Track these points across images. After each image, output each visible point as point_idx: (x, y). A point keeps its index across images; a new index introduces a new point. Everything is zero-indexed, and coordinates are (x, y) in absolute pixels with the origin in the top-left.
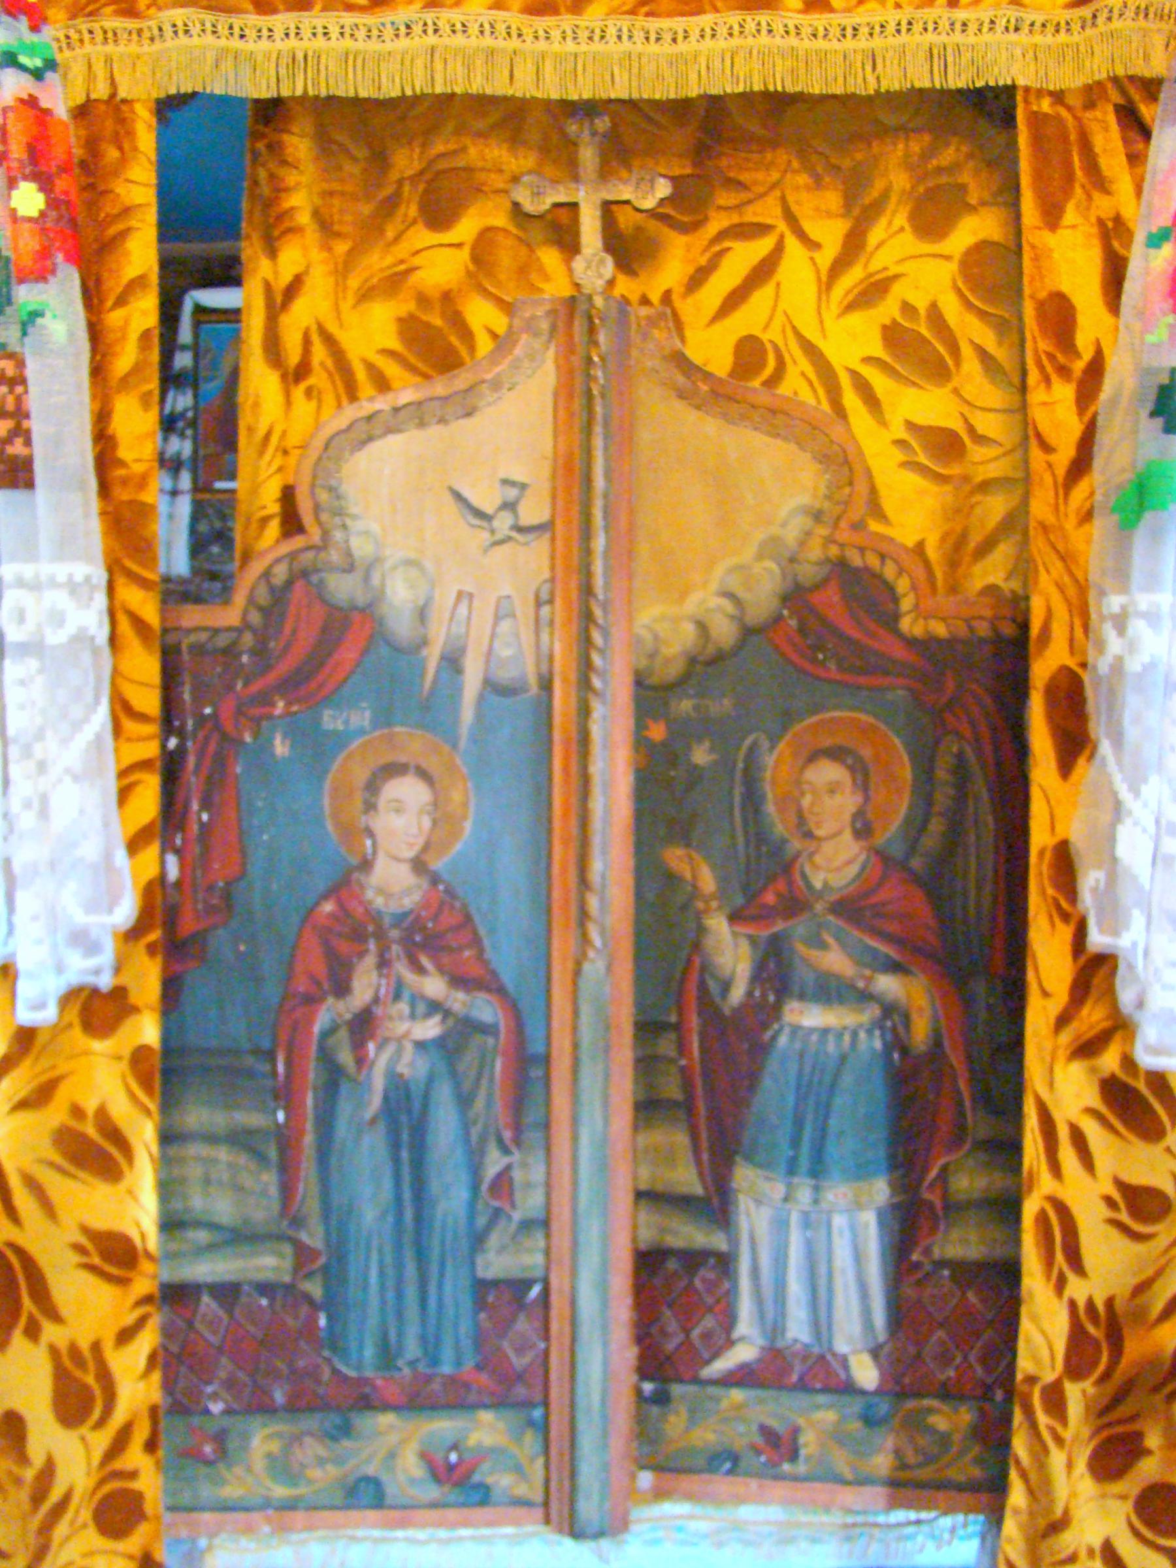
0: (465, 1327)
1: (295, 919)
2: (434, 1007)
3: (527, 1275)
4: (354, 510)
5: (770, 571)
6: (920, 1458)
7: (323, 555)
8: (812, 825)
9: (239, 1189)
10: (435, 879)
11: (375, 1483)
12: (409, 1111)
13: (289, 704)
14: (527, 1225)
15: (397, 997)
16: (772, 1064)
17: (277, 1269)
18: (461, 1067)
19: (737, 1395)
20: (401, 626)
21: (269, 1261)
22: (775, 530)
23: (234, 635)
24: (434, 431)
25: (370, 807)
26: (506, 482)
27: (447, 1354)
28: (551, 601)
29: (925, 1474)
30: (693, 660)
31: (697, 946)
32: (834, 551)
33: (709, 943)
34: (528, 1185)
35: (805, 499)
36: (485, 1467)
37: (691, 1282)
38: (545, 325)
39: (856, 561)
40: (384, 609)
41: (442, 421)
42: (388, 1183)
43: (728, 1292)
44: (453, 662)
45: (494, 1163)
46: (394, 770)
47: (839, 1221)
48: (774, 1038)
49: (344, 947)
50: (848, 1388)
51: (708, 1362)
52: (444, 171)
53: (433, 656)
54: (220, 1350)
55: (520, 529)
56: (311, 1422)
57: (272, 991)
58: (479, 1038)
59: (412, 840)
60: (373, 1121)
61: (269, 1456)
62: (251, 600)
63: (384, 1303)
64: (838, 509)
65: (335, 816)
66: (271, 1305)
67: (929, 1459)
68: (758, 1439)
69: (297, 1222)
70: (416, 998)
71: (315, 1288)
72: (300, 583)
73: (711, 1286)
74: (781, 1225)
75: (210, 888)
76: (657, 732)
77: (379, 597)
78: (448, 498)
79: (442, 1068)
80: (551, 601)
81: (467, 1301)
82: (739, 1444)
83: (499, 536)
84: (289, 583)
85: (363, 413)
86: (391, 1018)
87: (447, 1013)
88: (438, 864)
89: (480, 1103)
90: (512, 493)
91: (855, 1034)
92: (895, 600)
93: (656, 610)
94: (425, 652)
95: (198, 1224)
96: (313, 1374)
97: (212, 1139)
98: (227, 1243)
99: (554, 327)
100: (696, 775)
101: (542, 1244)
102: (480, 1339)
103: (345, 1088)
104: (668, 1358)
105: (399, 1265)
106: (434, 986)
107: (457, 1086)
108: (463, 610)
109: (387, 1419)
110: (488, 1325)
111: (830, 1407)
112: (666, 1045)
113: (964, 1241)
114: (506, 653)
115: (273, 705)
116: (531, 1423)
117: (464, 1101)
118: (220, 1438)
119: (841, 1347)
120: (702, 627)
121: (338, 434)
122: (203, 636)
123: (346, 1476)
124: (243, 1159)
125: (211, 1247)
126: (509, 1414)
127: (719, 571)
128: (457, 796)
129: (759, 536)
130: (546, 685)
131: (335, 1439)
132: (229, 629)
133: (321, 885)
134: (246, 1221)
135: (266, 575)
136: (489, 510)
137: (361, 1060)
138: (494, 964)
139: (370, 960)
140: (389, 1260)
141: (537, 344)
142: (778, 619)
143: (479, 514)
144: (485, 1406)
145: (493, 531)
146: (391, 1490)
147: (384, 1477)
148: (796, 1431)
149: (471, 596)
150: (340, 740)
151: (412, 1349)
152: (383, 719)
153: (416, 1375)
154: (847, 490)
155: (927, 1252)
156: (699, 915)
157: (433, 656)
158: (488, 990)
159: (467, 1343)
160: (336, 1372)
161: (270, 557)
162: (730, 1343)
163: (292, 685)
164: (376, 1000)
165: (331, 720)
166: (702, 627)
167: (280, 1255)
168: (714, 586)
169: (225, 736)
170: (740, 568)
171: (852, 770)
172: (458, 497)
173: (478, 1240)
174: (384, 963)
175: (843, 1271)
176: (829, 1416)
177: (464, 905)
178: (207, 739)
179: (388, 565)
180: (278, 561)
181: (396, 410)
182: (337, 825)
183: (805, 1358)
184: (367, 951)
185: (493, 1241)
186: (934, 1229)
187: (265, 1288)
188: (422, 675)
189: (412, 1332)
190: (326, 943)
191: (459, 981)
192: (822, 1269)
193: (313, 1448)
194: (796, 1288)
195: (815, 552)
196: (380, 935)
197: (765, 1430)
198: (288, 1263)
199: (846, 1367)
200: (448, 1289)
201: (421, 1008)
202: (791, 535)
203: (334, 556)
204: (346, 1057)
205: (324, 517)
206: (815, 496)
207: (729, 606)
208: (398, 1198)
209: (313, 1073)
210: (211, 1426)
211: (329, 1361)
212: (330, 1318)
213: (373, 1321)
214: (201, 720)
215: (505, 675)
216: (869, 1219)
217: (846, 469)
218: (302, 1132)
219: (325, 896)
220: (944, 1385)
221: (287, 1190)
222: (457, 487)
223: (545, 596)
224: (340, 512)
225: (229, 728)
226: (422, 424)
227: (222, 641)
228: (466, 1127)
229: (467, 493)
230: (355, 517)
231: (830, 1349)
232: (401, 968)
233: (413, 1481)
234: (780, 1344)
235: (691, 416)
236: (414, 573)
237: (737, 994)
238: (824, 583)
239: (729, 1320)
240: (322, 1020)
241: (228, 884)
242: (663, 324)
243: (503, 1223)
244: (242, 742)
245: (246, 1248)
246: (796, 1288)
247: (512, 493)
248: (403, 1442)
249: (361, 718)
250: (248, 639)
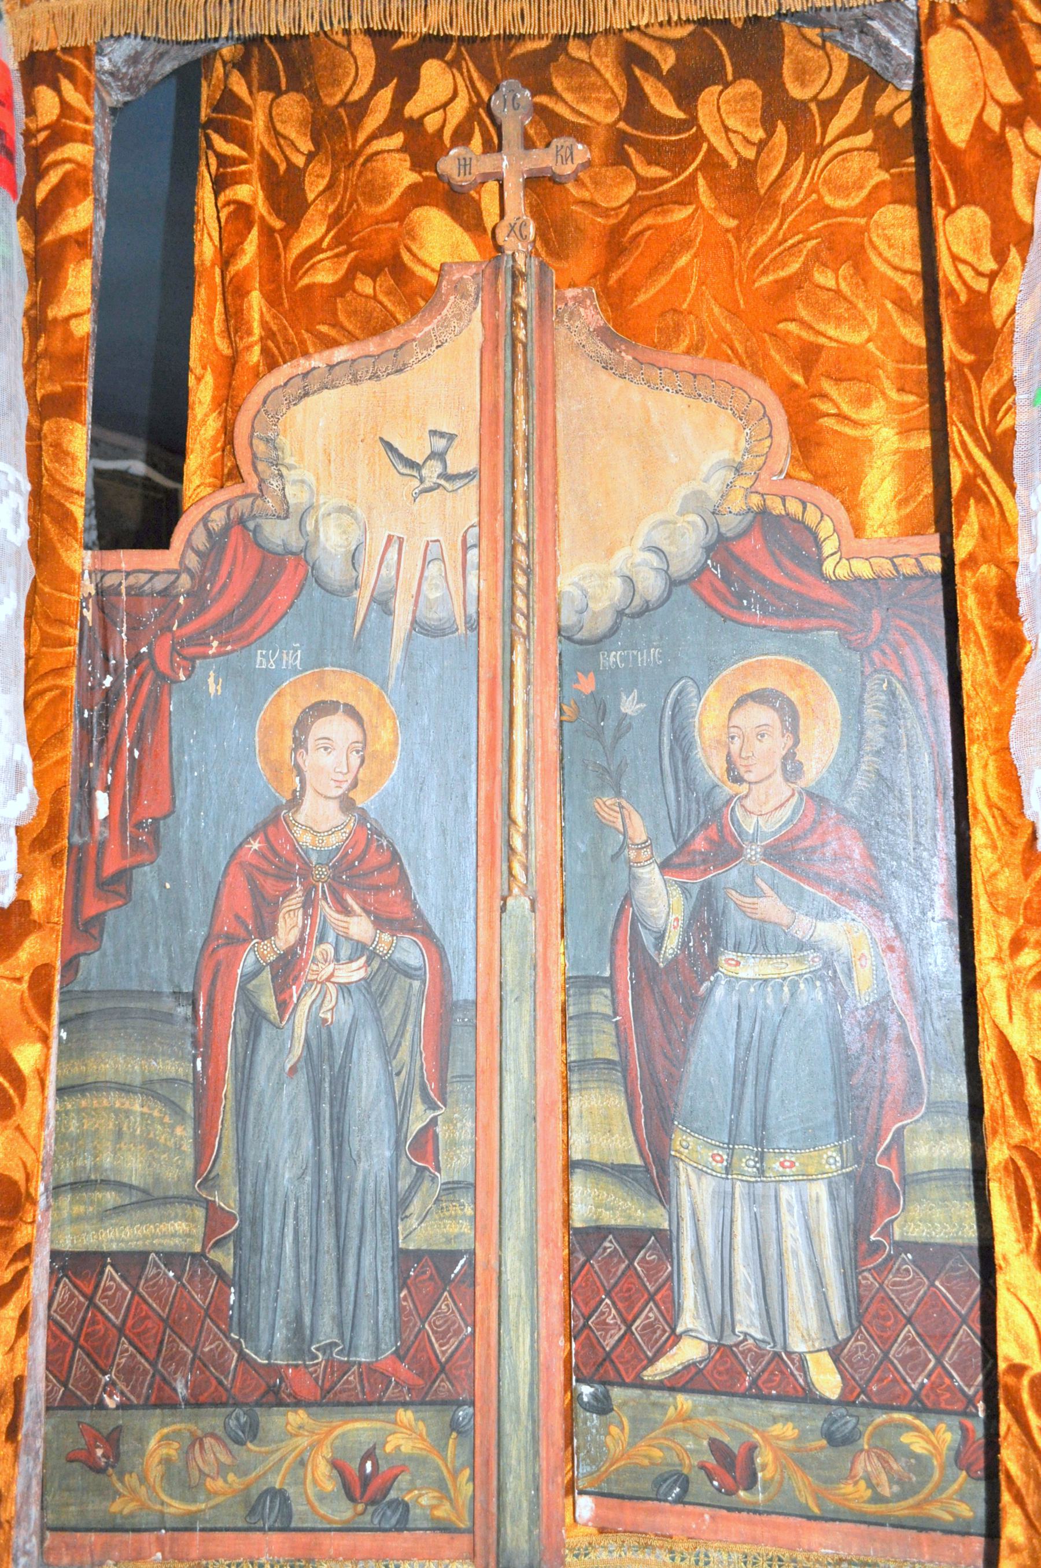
0: (386, 1305)
1: (223, 859)
2: (360, 949)
3: (454, 1246)
4: (289, 460)
5: (693, 524)
6: (896, 1488)
7: (259, 502)
8: (742, 770)
9: (151, 1144)
10: (363, 816)
11: (280, 1496)
12: (331, 1059)
13: (223, 644)
14: (452, 1188)
15: (321, 940)
16: (710, 1019)
17: (188, 1235)
18: (386, 1013)
19: (684, 1401)
20: (334, 571)
21: (180, 1226)
22: (696, 485)
23: (173, 577)
24: (367, 386)
25: (299, 744)
26: (433, 433)
27: (365, 1338)
28: (478, 545)
29: (900, 1509)
30: (620, 613)
31: (628, 898)
32: (755, 500)
33: (640, 893)
34: (453, 1143)
35: (726, 454)
36: (404, 1479)
37: (631, 1265)
38: (472, 288)
39: (776, 507)
40: (316, 554)
41: (375, 376)
42: (307, 1141)
43: (670, 1276)
44: (383, 603)
45: (418, 1118)
46: (323, 709)
47: (787, 1193)
48: (710, 991)
49: (270, 886)
50: (808, 1396)
51: (652, 1361)
52: (377, 153)
53: (364, 597)
54: (121, 1330)
55: (450, 478)
56: (213, 1420)
57: (197, 933)
58: (402, 981)
59: (340, 777)
60: (293, 1070)
61: (167, 1461)
62: (188, 543)
63: (298, 1276)
64: (760, 461)
65: (265, 751)
66: (178, 1278)
67: (907, 1491)
68: (711, 1460)
69: (209, 1181)
70: (344, 937)
71: (226, 1259)
72: (236, 530)
73: (652, 1270)
74: (725, 1200)
75: (139, 825)
76: (587, 685)
77: (310, 543)
78: (380, 448)
79: (366, 1014)
80: (478, 545)
81: (387, 1277)
82: (689, 1465)
83: (427, 484)
84: (226, 530)
85: (300, 370)
86: (315, 961)
87: (373, 955)
88: (362, 801)
89: (404, 1054)
90: (441, 444)
91: (794, 985)
92: (818, 545)
93: (584, 568)
94: (356, 594)
95: (106, 1183)
96: (219, 1360)
97: (125, 1088)
98: (140, 1204)
99: (480, 289)
100: (623, 725)
101: (469, 1211)
102: (400, 1321)
103: (266, 1031)
104: (608, 1355)
105: (316, 1232)
106: (360, 927)
107: (381, 1037)
108: (392, 554)
109: (297, 1417)
110: (409, 1305)
111: (787, 1419)
112: (600, 1002)
113: (927, 1220)
114: (434, 595)
115: (209, 645)
116: (455, 1426)
117: (388, 1050)
118: (113, 1440)
119: (797, 1345)
120: (629, 580)
121: (276, 389)
122: (144, 578)
123: (247, 1488)
124: (156, 1111)
125: (118, 1209)
126: (429, 1412)
127: (644, 528)
128: (386, 735)
129: (683, 491)
130: (473, 625)
131: (240, 1443)
132: (169, 572)
133: (250, 825)
134: (157, 1180)
135: (205, 520)
136: (420, 461)
137: (282, 1006)
138: (421, 904)
139: (296, 899)
140: (304, 1227)
141: (464, 304)
142: (703, 569)
143: (411, 464)
144: (405, 1404)
145: (422, 481)
146: (299, 1507)
147: (291, 1491)
148: (752, 1449)
149: (401, 540)
150: (272, 679)
151: (327, 1332)
152: (316, 660)
153: (330, 1362)
154: (767, 442)
155: (886, 1231)
156: (629, 864)
157: (364, 597)
158: (412, 931)
159: (386, 1326)
160: (242, 1356)
161: (208, 504)
162: (676, 1338)
163: (223, 627)
164: (301, 941)
165: (262, 659)
166: (629, 580)
167: (192, 1220)
168: (639, 542)
169: (162, 676)
170: (663, 523)
171: (779, 711)
172: (389, 447)
173: (401, 1205)
174: (309, 903)
175: (795, 1254)
176: (787, 1431)
177: (391, 844)
178: (142, 677)
179: (322, 511)
180: (216, 507)
181: (331, 367)
182: (267, 761)
183: (757, 1359)
184: (292, 891)
185: (415, 1207)
186: (893, 1204)
187: (170, 1258)
188: (354, 616)
189: (328, 1311)
190: (251, 880)
191: (382, 922)
192: (772, 1251)
193: (215, 1453)
194: (744, 1273)
195: (737, 502)
196: (306, 871)
197: (716, 1446)
198: (199, 1231)
199: (803, 1368)
200: (367, 1260)
201: (345, 952)
202: (713, 489)
203: (270, 503)
204: (268, 1002)
205: (261, 467)
206: (736, 450)
207: (654, 560)
208: (318, 1153)
209: (234, 1019)
210: (106, 1424)
211: (236, 1344)
212: (240, 1294)
213: (286, 1297)
214: (136, 659)
215: (433, 616)
216: (820, 1190)
217: (765, 421)
218: (219, 1082)
219: (253, 835)
220: (916, 1396)
221: (203, 1145)
222: (386, 439)
223: (471, 540)
224: (276, 463)
225: (163, 665)
226: (355, 380)
227: (159, 583)
228: (390, 1075)
229: (396, 445)
230: (289, 467)
231: (785, 1347)
232: (327, 909)
233: (322, 1497)
234: (729, 1341)
235: (618, 383)
236: (346, 518)
237: (672, 944)
238: (744, 534)
239: (672, 1311)
240: (247, 961)
241: (156, 820)
242: (588, 302)
243: (426, 1184)
244: (178, 681)
245: (154, 1212)
246: (744, 1273)
247: (441, 444)
248: (314, 1446)
249: (293, 658)
250: (185, 582)
